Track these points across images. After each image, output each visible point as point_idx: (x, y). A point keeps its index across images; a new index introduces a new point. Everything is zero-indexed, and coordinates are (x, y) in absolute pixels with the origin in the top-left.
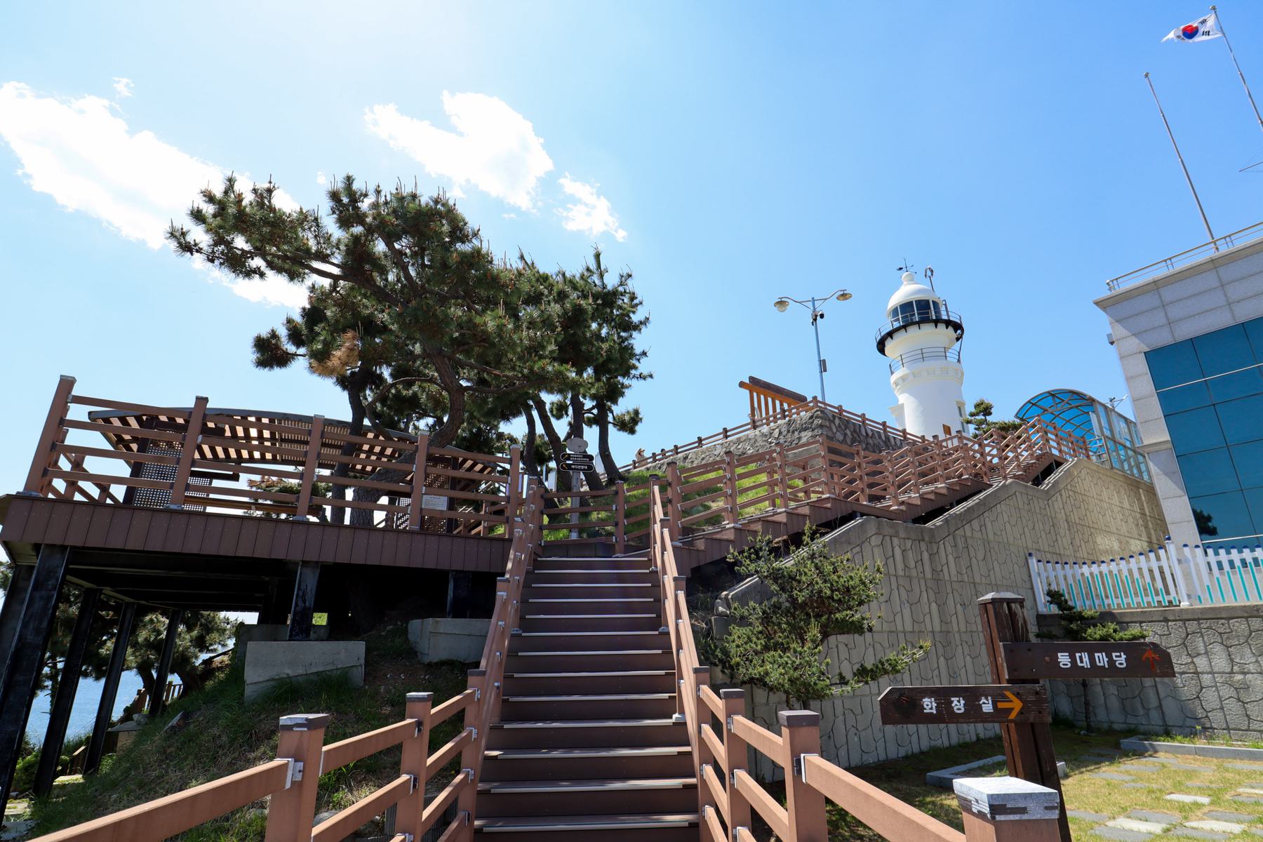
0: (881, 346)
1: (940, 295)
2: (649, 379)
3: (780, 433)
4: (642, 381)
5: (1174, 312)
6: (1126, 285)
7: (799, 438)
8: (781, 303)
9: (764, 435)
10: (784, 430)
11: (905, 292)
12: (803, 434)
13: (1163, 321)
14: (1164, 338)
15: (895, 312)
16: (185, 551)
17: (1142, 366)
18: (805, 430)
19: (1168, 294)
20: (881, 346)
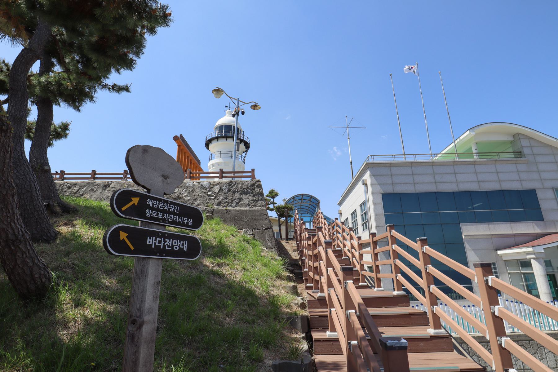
0: (207, 145)
1: (243, 127)
2: (124, 93)
3: (221, 190)
4: (114, 94)
5: (438, 178)
6: (377, 160)
7: (240, 199)
8: (218, 91)
9: (202, 187)
10: (225, 188)
11: (227, 119)
12: (244, 196)
13: (391, 182)
14: (390, 190)
15: (221, 127)
16: (539, 201)
17: (380, 200)
18: (246, 193)
19: (395, 170)
20: (207, 145)
